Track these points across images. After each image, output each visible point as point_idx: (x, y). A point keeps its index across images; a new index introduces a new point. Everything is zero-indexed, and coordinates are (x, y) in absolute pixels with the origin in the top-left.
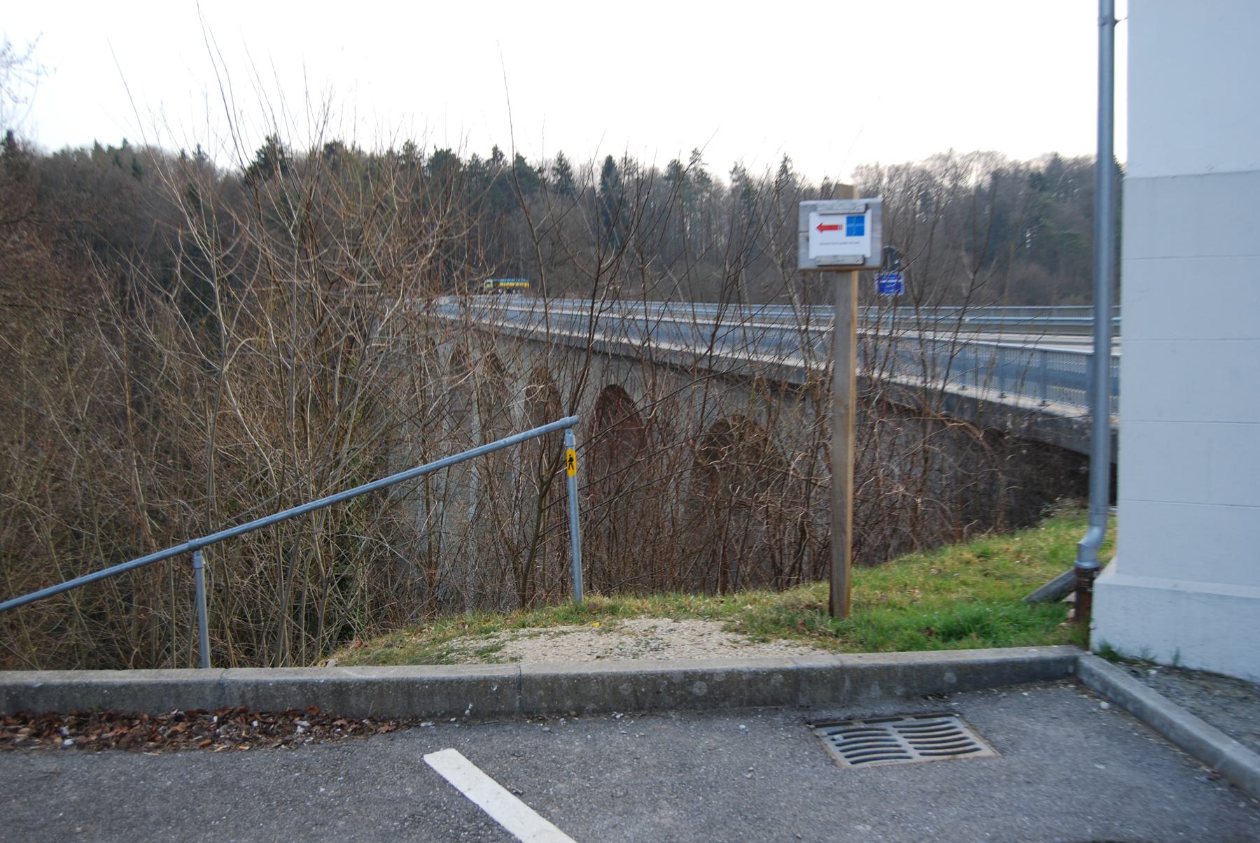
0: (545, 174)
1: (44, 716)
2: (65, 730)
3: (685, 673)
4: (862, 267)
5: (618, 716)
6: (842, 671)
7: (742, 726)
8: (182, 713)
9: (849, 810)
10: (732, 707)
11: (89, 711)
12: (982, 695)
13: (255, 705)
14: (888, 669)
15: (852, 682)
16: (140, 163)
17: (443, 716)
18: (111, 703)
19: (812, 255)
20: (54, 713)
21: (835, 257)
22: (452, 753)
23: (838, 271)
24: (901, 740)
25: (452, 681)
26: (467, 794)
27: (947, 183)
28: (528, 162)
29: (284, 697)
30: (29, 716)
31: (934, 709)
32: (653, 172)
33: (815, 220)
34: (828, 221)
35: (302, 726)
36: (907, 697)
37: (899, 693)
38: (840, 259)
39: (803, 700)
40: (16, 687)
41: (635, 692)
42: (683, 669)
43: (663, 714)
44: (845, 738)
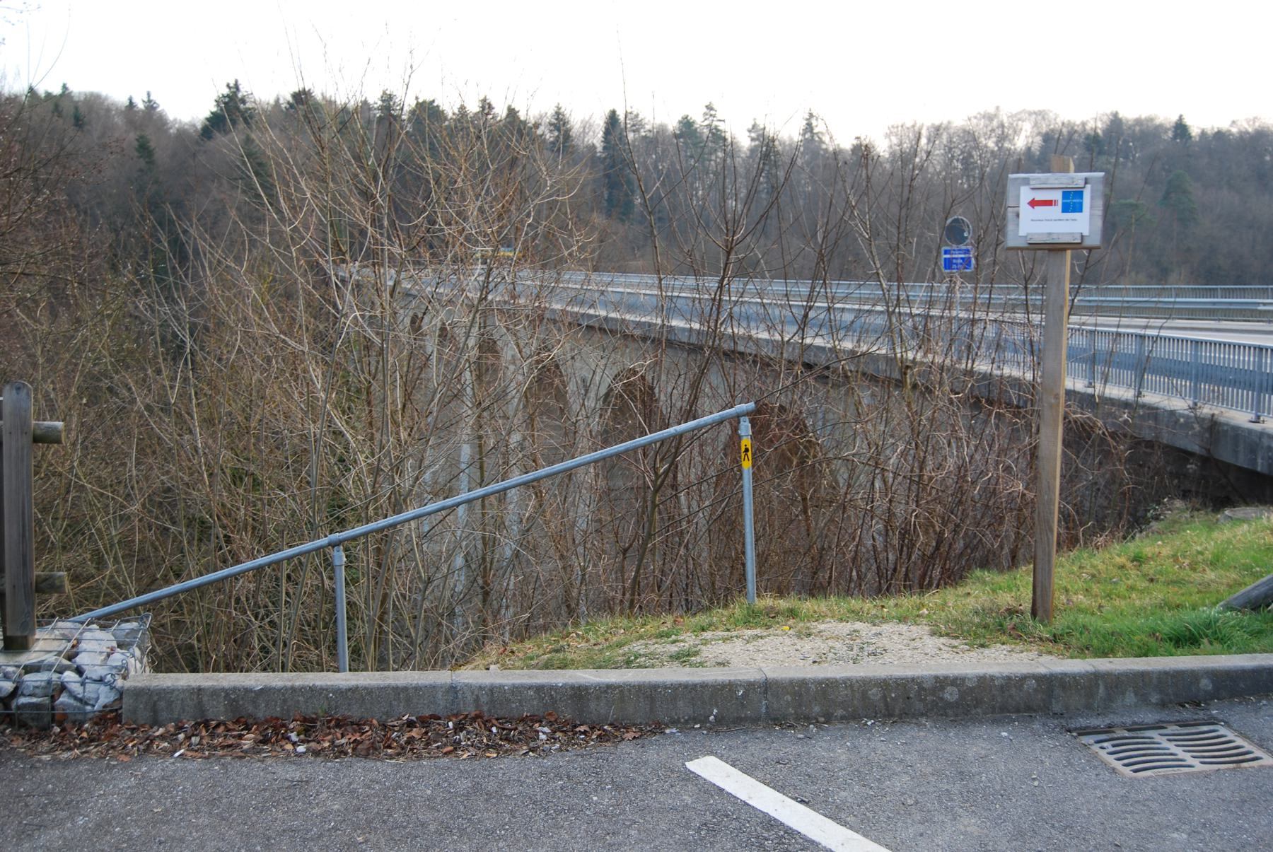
1: (267, 721)
2: (294, 736)
3: (936, 677)
5: (869, 723)
6: (1096, 677)
7: (1004, 734)
8: (414, 718)
9: (1155, 818)
10: (985, 714)
11: (314, 716)
12: (1240, 703)
13: (489, 711)
14: (1143, 675)
15: (1106, 688)
16: (83, 110)
17: (687, 722)
18: (336, 707)
19: (1022, 233)
20: (277, 719)
22: (711, 760)
23: (1050, 250)
24: (1172, 747)
25: (696, 685)
26: (750, 802)
27: (991, 144)
28: (522, 116)
29: (520, 701)
30: (250, 721)
31: (1196, 717)
33: (1026, 195)
34: (1040, 196)
35: (544, 733)
36: (1163, 705)
37: (1153, 701)
38: (1055, 237)
39: (1057, 707)
40: (235, 689)
41: (884, 697)
42: (933, 673)
43: (914, 721)
44: (1114, 746)
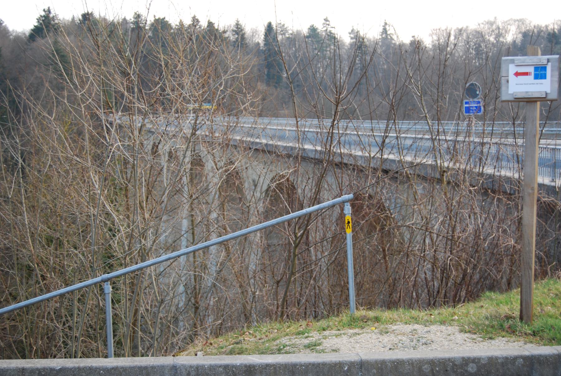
0: (226, 35)
3: (463, 358)
4: (543, 99)
19: (511, 91)
21: (527, 92)
23: (527, 102)
25: (319, 364)
27: (492, 39)
32: (298, 33)
33: (512, 69)
38: (530, 94)
42: (461, 355)
